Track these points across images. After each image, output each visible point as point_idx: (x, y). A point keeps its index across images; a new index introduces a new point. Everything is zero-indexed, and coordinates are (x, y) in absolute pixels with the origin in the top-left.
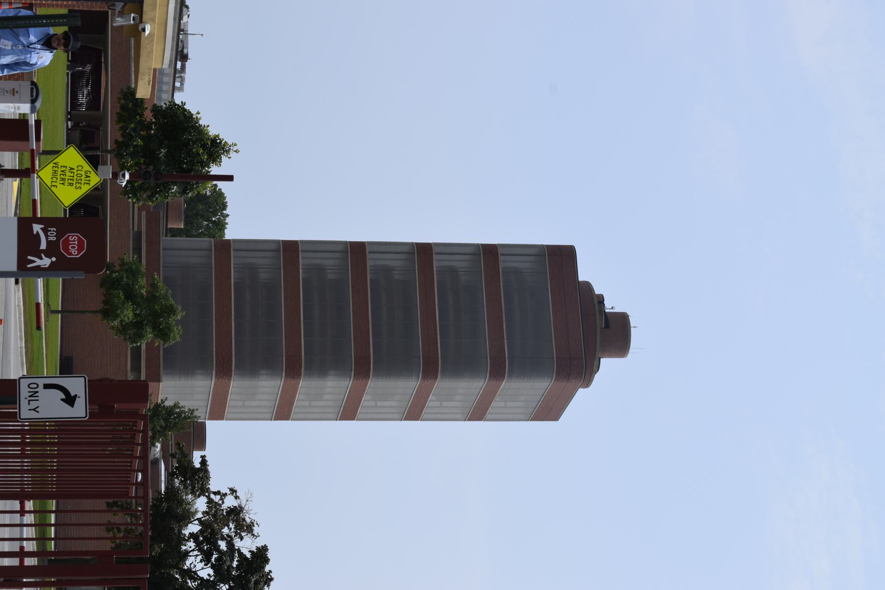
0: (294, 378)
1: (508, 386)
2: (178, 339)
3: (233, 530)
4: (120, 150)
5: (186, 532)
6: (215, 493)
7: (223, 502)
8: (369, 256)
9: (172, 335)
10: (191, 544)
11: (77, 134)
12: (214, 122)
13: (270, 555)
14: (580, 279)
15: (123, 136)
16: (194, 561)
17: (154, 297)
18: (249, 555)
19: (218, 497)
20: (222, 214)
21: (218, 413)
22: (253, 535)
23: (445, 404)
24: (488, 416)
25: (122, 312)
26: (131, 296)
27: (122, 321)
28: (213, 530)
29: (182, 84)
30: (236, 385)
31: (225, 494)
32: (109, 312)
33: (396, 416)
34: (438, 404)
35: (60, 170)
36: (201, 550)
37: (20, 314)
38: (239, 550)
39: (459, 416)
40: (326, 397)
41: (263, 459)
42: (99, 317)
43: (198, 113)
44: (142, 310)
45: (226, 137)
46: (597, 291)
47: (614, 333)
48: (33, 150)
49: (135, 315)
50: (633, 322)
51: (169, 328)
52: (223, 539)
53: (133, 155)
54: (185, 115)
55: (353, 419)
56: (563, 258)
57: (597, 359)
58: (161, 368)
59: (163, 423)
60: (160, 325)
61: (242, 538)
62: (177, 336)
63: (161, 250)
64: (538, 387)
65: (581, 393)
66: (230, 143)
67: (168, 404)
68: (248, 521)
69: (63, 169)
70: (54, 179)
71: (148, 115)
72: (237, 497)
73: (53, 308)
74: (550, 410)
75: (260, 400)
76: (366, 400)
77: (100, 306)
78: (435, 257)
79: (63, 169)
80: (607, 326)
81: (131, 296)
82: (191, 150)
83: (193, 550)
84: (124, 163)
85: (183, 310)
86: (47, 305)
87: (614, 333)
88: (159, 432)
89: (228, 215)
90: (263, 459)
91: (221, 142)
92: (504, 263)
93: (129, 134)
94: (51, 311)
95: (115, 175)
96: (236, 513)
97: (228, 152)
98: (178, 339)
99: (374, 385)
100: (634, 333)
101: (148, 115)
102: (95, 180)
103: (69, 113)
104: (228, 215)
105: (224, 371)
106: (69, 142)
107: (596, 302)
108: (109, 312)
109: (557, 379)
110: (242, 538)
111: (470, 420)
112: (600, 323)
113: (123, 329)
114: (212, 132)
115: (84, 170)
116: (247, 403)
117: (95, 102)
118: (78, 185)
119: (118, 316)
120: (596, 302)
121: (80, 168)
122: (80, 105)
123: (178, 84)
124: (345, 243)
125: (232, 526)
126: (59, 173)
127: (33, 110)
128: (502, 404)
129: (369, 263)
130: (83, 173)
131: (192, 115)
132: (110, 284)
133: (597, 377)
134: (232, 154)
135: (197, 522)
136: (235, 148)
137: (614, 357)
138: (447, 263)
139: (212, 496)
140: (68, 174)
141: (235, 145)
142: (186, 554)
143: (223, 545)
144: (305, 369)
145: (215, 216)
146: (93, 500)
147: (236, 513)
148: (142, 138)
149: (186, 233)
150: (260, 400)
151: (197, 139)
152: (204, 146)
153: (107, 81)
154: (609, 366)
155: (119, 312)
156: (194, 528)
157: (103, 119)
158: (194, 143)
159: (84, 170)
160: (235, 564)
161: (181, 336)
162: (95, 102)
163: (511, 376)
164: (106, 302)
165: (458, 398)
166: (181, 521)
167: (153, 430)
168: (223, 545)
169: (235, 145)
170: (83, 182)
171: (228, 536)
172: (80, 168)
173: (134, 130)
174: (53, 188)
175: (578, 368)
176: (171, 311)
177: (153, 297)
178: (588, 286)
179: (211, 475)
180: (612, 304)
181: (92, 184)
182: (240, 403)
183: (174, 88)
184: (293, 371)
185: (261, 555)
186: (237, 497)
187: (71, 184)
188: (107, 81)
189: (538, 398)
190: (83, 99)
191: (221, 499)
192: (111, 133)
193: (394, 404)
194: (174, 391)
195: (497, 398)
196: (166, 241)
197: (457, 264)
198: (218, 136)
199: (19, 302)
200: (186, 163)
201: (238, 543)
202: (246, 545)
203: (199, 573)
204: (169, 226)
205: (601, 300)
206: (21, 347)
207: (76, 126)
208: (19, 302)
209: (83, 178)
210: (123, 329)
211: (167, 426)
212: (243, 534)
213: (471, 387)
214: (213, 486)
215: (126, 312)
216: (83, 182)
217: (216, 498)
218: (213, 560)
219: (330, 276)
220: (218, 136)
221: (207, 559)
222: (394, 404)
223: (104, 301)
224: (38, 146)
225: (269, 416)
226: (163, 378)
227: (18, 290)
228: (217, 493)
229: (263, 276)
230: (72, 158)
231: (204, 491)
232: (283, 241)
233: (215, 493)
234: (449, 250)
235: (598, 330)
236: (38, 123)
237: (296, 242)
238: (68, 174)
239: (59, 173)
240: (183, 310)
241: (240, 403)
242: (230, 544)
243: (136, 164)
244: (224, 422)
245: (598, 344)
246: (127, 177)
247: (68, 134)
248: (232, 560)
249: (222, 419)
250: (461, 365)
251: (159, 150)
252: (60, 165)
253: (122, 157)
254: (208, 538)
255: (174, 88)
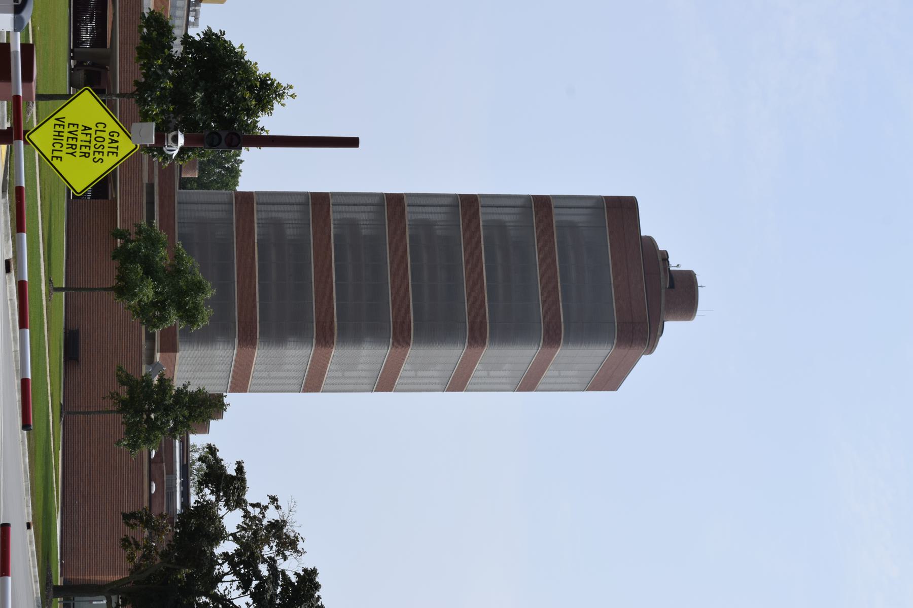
0: (325, 346)
1: (564, 353)
2: (207, 322)
3: (274, 548)
4: (143, 91)
5: (218, 550)
6: (253, 505)
7: (264, 517)
8: (407, 209)
9: (200, 317)
10: (226, 568)
11: (81, 74)
12: (263, 59)
13: (319, 579)
14: (643, 234)
15: (145, 75)
16: (229, 587)
17: (179, 271)
18: (294, 579)
19: (258, 510)
20: (235, 160)
21: (240, 384)
22: (298, 552)
23: (492, 373)
24: (539, 386)
25: (141, 290)
26: (150, 270)
27: (140, 301)
28: (253, 553)
29: (196, 19)
30: (261, 354)
31: (266, 508)
32: (124, 289)
33: (438, 387)
34: (484, 373)
35: (66, 130)
36: (237, 573)
37: (13, 310)
38: (283, 572)
39: (508, 387)
40: (360, 367)
41: (298, 442)
42: (113, 295)
43: (242, 47)
44: (164, 288)
45: (279, 77)
46: (661, 247)
47: (681, 294)
48: (17, 99)
49: (156, 293)
50: (700, 281)
51: (196, 307)
52: (264, 561)
53: (160, 101)
54: (225, 48)
55: (390, 391)
56: (623, 210)
57: (661, 324)
58: (178, 337)
59: (186, 413)
60: (186, 304)
61: (285, 558)
62: (206, 318)
63: (176, 204)
64: (596, 355)
65: (645, 360)
66: (284, 85)
67: (192, 389)
68: (292, 535)
69: (72, 128)
70: (58, 146)
71: (177, 48)
72: (277, 507)
73: (56, 285)
74: (608, 379)
75: (288, 370)
76: (406, 370)
77: (113, 282)
78: (481, 210)
79: (72, 128)
80: (672, 286)
81: (150, 270)
82: (234, 94)
83: (227, 574)
84: (148, 111)
85: (213, 287)
86: (49, 281)
87: (681, 294)
88: (182, 422)
89: (242, 161)
90: (298, 442)
91: (272, 84)
92: (558, 216)
93: (155, 72)
94: (53, 289)
95: (160, 138)
96: (277, 527)
97: (281, 96)
98: (207, 322)
99: (415, 353)
100: (702, 293)
101: (177, 48)
102: (126, 146)
103: (72, 51)
104: (242, 161)
105: (247, 339)
106: (76, 84)
107: (660, 259)
108: (124, 289)
109: (618, 346)
110: (285, 558)
111: (519, 390)
112: (665, 283)
113: (142, 311)
114: (261, 70)
115: (108, 130)
116: (273, 374)
117: (100, 38)
118: (98, 156)
119: (135, 295)
120: (660, 259)
121: (101, 127)
122: (84, 42)
123: (192, 19)
124: (381, 195)
125: (274, 544)
126: (66, 135)
127: (19, 24)
128: (556, 373)
129: (408, 217)
130: (106, 135)
131: (234, 49)
132: (125, 256)
133: (662, 340)
134: (287, 100)
135: (231, 538)
136: (291, 92)
137: (676, 320)
138: (495, 217)
139: (250, 509)
140: (81, 137)
141: (291, 87)
142: (219, 578)
143: (264, 569)
144: (338, 334)
145: (228, 162)
146: (55, 93)
147: (277, 527)
148: (171, 78)
149: (201, 184)
150: (288, 370)
151: (242, 79)
152: (251, 88)
153: (114, 15)
154: (673, 330)
155: (137, 290)
156: (229, 546)
157: (110, 57)
158: (239, 84)
159: (108, 130)
160: (279, 590)
161: (211, 319)
162: (100, 38)
163: (567, 342)
164: (121, 278)
165: (506, 367)
166: (213, 540)
167: (174, 420)
168: (264, 569)
169: (291, 87)
170: (106, 150)
171: (270, 558)
172: (101, 127)
173: (161, 67)
174: (55, 162)
175: (640, 334)
176: (199, 288)
177: (177, 272)
178: (650, 241)
179: (248, 484)
180: (678, 262)
181: (122, 153)
182: (265, 374)
183: (188, 23)
184: (325, 339)
185: (309, 579)
186: (277, 507)
187: (85, 155)
188: (114, 15)
189: (597, 366)
190: (86, 36)
191: (261, 513)
192: (125, 70)
193: (435, 374)
194: (193, 367)
195: (550, 367)
196: (180, 194)
197: (506, 218)
198: (268, 75)
199: (11, 295)
200: (228, 111)
201: (281, 565)
202: (291, 566)
203: (235, 602)
204: (183, 176)
205: (665, 256)
206: (16, 351)
207: (79, 64)
208: (11, 295)
209: (106, 144)
210: (142, 311)
211: (190, 415)
212: (287, 553)
213: (524, 355)
214: (250, 496)
215: (145, 290)
216: (106, 150)
217: (255, 512)
218: (253, 586)
219: (364, 232)
220: (268, 75)
221: (245, 585)
222: (435, 374)
223: (118, 276)
224: (27, 91)
225: (297, 387)
226: (181, 347)
227: (10, 280)
228: (257, 505)
229: (290, 232)
230: (86, 108)
231: (240, 503)
232: (311, 193)
233: (253, 505)
234: (497, 202)
235: (663, 291)
236: (27, 50)
237: (327, 194)
238: (81, 137)
239: (66, 135)
240: (213, 287)
241: (265, 374)
242: (272, 564)
243: (163, 112)
244: (247, 394)
245: (663, 306)
246: (181, 141)
247: (70, 74)
248: (275, 589)
249: (246, 391)
250: (512, 331)
251: (194, 94)
252: (67, 121)
253: (146, 102)
254: (245, 560)
255: (188, 23)
